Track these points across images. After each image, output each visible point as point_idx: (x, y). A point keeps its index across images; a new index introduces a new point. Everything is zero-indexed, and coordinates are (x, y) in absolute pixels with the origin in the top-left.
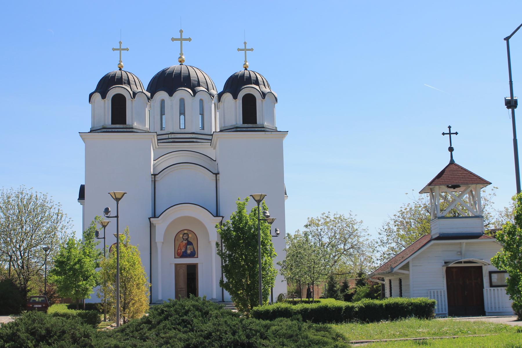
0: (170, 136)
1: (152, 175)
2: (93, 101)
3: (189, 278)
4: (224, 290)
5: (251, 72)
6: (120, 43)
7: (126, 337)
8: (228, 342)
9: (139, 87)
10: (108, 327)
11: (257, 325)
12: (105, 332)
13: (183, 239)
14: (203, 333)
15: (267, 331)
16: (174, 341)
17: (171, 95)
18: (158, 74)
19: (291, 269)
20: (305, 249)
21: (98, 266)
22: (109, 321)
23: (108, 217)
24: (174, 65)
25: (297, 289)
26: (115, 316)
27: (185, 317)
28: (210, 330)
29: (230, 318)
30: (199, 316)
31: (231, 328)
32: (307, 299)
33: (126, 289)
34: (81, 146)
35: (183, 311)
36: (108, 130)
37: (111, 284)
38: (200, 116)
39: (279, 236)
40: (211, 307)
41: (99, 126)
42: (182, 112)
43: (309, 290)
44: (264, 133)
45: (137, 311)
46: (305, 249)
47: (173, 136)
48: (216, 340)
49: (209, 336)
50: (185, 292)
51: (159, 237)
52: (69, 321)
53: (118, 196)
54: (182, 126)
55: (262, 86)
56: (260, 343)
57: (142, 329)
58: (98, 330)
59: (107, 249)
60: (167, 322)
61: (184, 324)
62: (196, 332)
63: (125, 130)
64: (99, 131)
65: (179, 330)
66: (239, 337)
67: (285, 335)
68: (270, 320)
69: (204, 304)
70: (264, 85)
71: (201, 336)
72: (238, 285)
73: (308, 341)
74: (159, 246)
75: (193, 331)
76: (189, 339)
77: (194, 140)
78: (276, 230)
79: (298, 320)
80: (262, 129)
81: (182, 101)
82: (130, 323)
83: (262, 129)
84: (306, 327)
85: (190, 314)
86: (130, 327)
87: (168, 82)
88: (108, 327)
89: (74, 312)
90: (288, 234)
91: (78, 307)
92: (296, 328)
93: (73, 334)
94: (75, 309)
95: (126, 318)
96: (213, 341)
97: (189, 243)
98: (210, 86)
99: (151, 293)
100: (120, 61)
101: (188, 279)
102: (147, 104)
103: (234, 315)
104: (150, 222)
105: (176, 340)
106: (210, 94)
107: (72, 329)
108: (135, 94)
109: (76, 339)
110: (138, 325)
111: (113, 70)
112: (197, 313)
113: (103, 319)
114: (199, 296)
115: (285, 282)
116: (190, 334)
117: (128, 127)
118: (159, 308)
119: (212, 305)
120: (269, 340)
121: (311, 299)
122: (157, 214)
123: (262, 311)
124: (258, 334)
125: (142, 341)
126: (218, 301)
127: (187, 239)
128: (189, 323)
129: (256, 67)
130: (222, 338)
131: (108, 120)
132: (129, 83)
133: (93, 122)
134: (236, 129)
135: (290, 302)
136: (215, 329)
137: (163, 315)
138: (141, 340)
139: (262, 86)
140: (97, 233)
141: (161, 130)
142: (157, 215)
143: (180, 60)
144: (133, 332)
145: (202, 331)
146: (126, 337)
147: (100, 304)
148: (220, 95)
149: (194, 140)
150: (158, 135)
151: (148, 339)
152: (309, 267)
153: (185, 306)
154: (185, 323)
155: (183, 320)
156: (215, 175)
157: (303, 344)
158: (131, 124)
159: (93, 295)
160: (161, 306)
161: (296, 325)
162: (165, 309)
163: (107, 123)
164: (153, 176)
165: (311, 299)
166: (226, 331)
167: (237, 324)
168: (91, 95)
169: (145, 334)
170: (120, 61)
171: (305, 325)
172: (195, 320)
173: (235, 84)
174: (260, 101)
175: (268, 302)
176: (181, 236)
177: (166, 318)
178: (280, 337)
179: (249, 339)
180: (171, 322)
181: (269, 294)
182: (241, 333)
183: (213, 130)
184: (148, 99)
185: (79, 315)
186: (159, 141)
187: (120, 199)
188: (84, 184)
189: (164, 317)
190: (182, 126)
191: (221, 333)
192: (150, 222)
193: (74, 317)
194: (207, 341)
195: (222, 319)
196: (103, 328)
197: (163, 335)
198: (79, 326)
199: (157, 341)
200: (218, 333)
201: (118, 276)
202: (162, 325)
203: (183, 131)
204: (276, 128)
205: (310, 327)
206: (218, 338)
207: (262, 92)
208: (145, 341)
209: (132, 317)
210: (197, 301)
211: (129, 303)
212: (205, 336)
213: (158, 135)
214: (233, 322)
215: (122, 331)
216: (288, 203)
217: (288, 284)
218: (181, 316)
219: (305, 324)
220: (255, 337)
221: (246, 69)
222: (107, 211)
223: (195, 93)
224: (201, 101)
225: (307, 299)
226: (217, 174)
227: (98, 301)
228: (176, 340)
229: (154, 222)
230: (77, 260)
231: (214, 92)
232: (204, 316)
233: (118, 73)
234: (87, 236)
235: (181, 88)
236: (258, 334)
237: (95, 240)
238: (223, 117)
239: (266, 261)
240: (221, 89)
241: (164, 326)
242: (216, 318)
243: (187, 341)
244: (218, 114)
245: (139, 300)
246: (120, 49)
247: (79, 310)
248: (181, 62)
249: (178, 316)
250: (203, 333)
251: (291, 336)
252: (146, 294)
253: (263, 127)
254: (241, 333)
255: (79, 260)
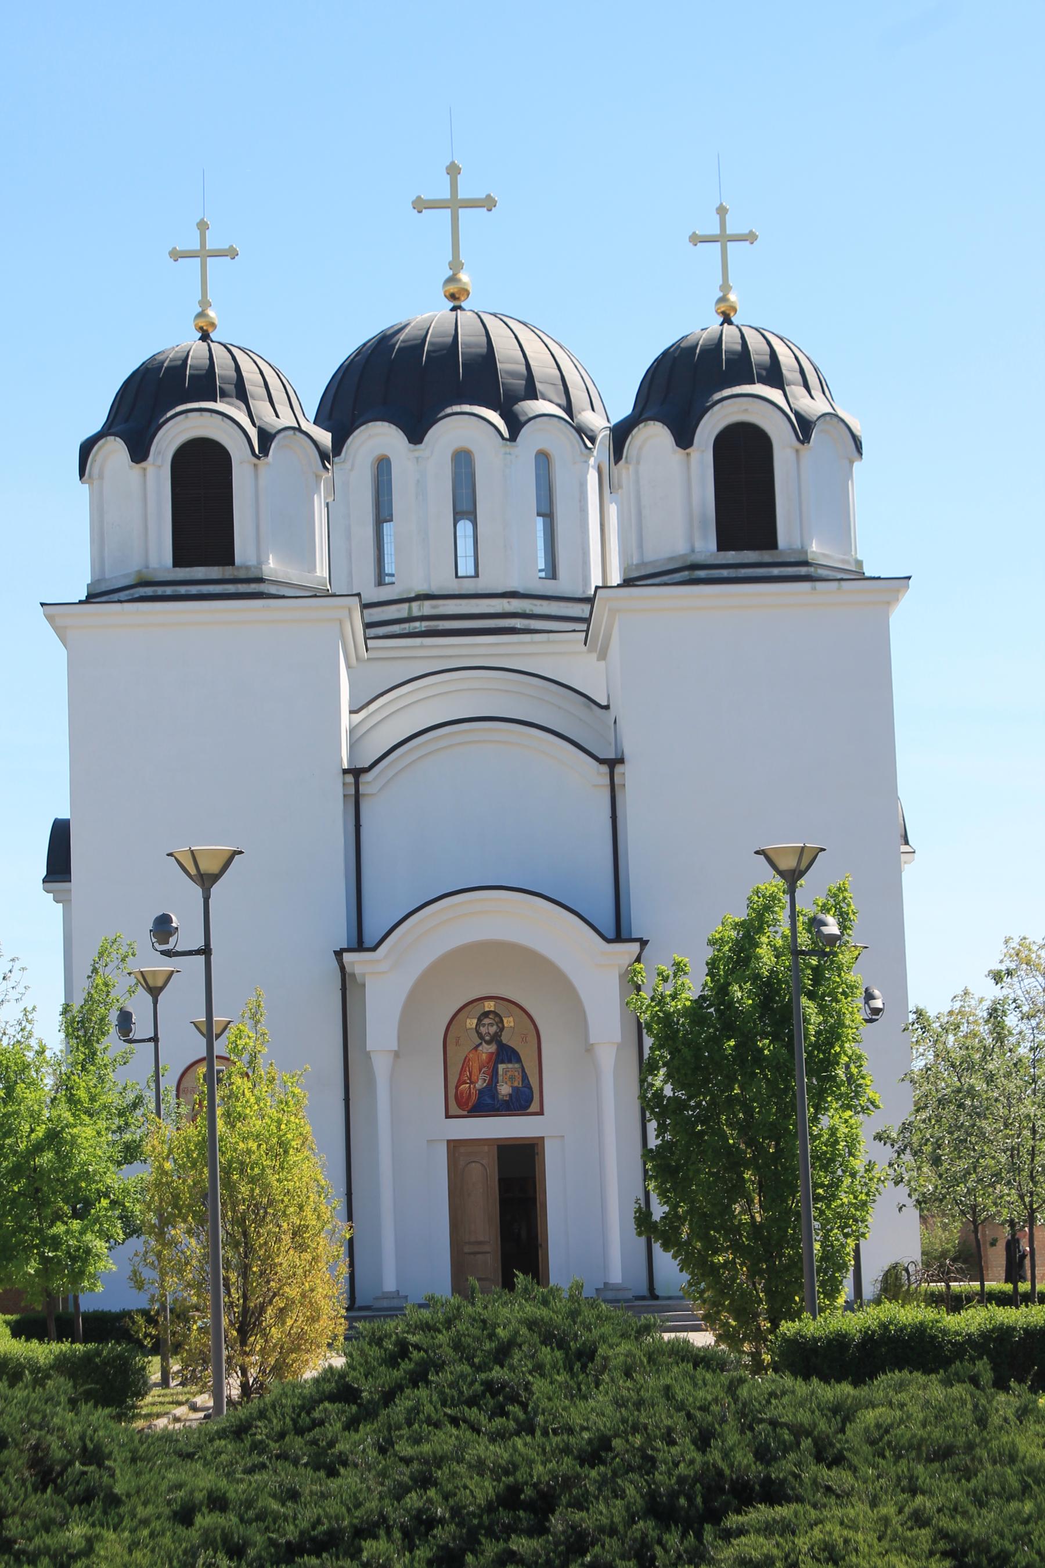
0: (416, 609)
1: (345, 772)
2: (96, 471)
3: (509, 1201)
4: (657, 1247)
5: (749, 333)
6: (203, 226)
7: (256, 1459)
8: (681, 1480)
9: (283, 408)
10: (181, 1411)
11: (801, 1404)
12: (167, 1437)
13: (481, 1036)
14: (572, 1440)
15: (842, 1430)
16: (454, 1475)
17: (416, 435)
18: (359, 352)
19: (936, 1161)
20: (990, 1078)
21: (131, 1153)
22: (183, 1384)
23: (167, 953)
24: (418, 309)
25: (963, 1243)
26: (207, 1365)
27: (497, 1373)
28: (603, 1424)
29: (686, 1374)
30: (554, 1366)
31: (689, 1416)
32: (1008, 1287)
33: (249, 1250)
34: (55, 655)
35: (488, 1346)
36: (160, 590)
37: (189, 1232)
38: (540, 520)
39: (882, 1019)
40: (607, 1329)
41: (121, 574)
42: (465, 509)
43: (1012, 1245)
44: (806, 586)
45: (298, 1343)
46: (990, 1078)
47: (427, 608)
48: (630, 1469)
49: (597, 1452)
50: (490, 1260)
51: (381, 1031)
52: (20, 1393)
53: (209, 866)
54: (466, 567)
55: (797, 391)
56: (815, 1482)
57: (322, 1423)
58: (140, 1424)
59: (169, 1083)
60: (422, 1393)
61: (492, 1402)
62: (545, 1433)
63: (231, 588)
64: (122, 595)
65: (476, 1429)
66: (726, 1455)
67: (919, 1448)
68: (855, 1384)
69: (573, 1314)
70: (806, 386)
71: (566, 1450)
72: (712, 1222)
73: (1020, 1472)
74: (381, 1066)
75: (532, 1432)
76: (516, 1467)
77: (518, 623)
78: (869, 996)
79: (974, 1380)
80: (801, 570)
81: (463, 463)
82: (268, 1398)
83: (801, 570)
84: (1010, 1413)
85: (517, 1355)
86: (270, 1413)
87: (403, 383)
88: (181, 1411)
89: (41, 1352)
90: (919, 1013)
91: (52, 1327)
92: (965, 1417)
93: (36, 1448)
94: (41, 1340)
95: (253, 1372)
96: (615, 1474)
97: (506, 1054)
98: (578, 396)
99: (352, 1265)
100: (205, 303)
101: (505, 1203)
102: (318, 478)
103: (701, 1360)
104: (342, 968)
105: (462, 1469)
106: (580, 430)
107: (33, 1425)
108: (266, 438)
109: (51, 1470)
110: (302, 1407)
111: (173, 338)
112: (547, 1354)
113: (156, 1377)
114: (553, 1281)
115: (913, 1214)
116: (519, 1442)
117: (242, 575)
118: (388, 1336)
119: (608, 1318)
120: (854, 1470)
121: (1024, 1287)
122: (371, 936)
123: (815, 1340)
124: (806, 1443)
125: (322, 1474)
126: (630, 1295)
127: (496, 1038)
128: (514, 1399)
129: (769, 314)
130: (652, 1460)
131: (158, 551)
132: (241, 393)
133: (98, 560)
134: (689, 573)
135: (934, 1300)
136: (624, 1421)
137: (406, 1366)
138: (317, 1468)
139: (797, 391)
140: (125, 1020)
141: (380, 582)
142: (369, 940)
143: (452, 288)
144: (282, 1436)
145: (570, 1431)
146: (256, 1459)
147: (145, 1313)
148: (621, 433)
149: (518, 623)
150: (365, 606)
151: (345, 1464)
152: (1013, 1152)
153: (495, 1325)
154: (500, 1398)
155: (488, 1385)
156: (605, 769)
157: (996, 1487)
158: (252, 561)
159: (111, 1275)
160: (394, 1327)
161: (964, 1403)
162: (413, 1339)
163: (154, 563)
164: (350, 779)
165: (1024, 1287)
166: (670, 1430)
167: (716, 1400)
168: (86, 449)
169: (331, 1444)
170: (205, 303)
171: (1004, 1404)
172: (539, 1385)
173: (683, 383)
174: (790, 454)
175: (841, 1301)
176: (472, 1023)
177: (418, 1378)
178: (898, 1457)
179: (768, 1464)
180: (442, 1393)
181: (844, 1266)
182: (732, 1438)
183: (596, 580)
184: (324, 456)
185: (61, 1364)
186: (373, 632)
187: (215, 877)
188: (65, 814)
189: (411, 1373)
190: (466, 567)
191: (649, 1439)
192: (342, 968)
193: (40, 1375)
194: (593, 1473)
195: (651, 1382)
196: (159, 1416)
197: (408, 1451)
198: (62, 1416)
199: (383, 1474)
200: (638, 1440)
201: (221, 1202)
202: (402, 1405)
203: (469, 586)
204: (859, 563)
205: (1023, 1412)
206: (637, 1461)
207: (797, 414)
208: (332, 1473)
209: (278, 1369)
210: (545, 1303)
211: (262, 1309)
212: (581, 1450)
213: (365, 606)
214: (701, 1394)
215: (240, 1431)
216: (915, 878)
217: (923, 1219)
218: (479, 1369)
219: (1002, 1397)
220: (792, 1456)
221: (727, 320)
222: (163, 927)
223: (515, 425)
224: (543, 459)
225: (1008, 1287)
226: (613, 763)
227: (132, 1301)
228: (462, 1469)
229: (358, 970)
230: (40, 1132)
231: (596, 421)
232: (577, 1366)
233: (198, 350)
234: (81, 1028)
235: (457, 408)
236: (806, 1443)
237: (111, 1044)
238: (635, 526)
239: (833, 1131)
240: (623, 407)
241: (409, 1411)
242: (628, 1374)
243: (507, 1473)
244: (613, 510)
245: (304, 1295)
246: (203, 254)
247: (59, 1340)
248: (456, 297)
249: (466, 1368)
250: (572, 1440)
251: (944, 1453)
252: (331, 1269)
253: (806, 563)
254: (732, 1438)
255: (54, 1137)
